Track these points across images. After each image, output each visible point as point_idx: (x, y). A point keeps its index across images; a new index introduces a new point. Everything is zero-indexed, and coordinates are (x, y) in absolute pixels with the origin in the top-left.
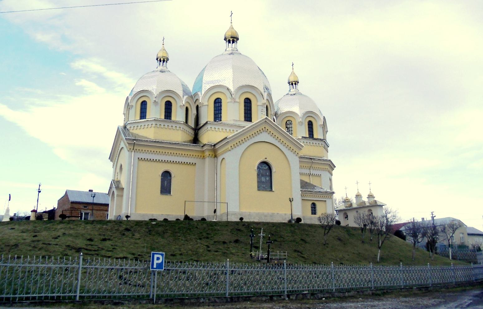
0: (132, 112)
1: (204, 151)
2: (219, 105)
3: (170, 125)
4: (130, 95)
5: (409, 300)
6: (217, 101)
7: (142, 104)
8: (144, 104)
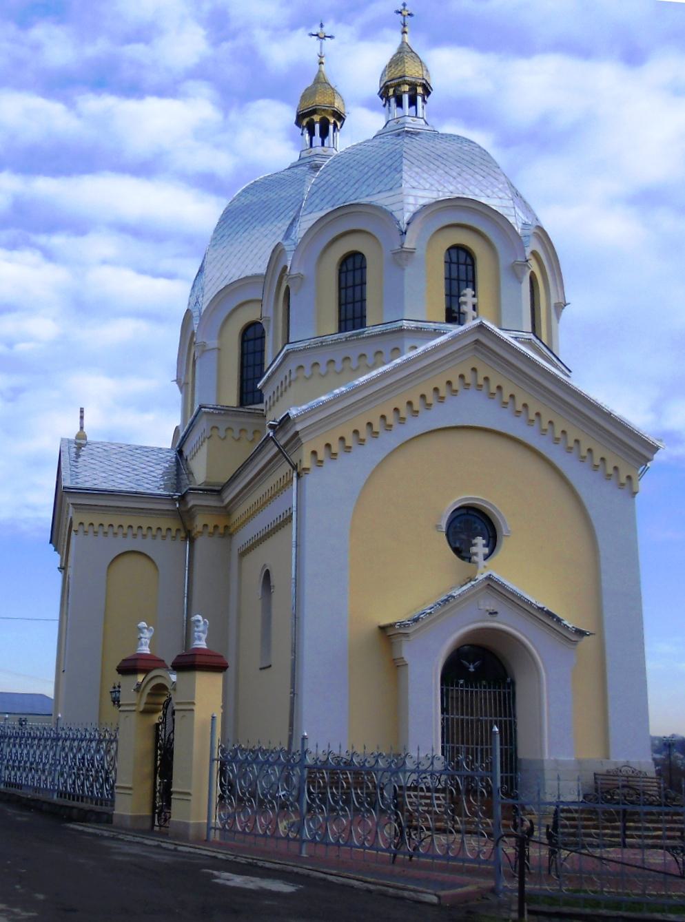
0: (206, 368)
1: (226, 507)
2: (358, 265)
4: (287, 236)
6: (250, 334)
7: (344, 268)
8: (350, 267)
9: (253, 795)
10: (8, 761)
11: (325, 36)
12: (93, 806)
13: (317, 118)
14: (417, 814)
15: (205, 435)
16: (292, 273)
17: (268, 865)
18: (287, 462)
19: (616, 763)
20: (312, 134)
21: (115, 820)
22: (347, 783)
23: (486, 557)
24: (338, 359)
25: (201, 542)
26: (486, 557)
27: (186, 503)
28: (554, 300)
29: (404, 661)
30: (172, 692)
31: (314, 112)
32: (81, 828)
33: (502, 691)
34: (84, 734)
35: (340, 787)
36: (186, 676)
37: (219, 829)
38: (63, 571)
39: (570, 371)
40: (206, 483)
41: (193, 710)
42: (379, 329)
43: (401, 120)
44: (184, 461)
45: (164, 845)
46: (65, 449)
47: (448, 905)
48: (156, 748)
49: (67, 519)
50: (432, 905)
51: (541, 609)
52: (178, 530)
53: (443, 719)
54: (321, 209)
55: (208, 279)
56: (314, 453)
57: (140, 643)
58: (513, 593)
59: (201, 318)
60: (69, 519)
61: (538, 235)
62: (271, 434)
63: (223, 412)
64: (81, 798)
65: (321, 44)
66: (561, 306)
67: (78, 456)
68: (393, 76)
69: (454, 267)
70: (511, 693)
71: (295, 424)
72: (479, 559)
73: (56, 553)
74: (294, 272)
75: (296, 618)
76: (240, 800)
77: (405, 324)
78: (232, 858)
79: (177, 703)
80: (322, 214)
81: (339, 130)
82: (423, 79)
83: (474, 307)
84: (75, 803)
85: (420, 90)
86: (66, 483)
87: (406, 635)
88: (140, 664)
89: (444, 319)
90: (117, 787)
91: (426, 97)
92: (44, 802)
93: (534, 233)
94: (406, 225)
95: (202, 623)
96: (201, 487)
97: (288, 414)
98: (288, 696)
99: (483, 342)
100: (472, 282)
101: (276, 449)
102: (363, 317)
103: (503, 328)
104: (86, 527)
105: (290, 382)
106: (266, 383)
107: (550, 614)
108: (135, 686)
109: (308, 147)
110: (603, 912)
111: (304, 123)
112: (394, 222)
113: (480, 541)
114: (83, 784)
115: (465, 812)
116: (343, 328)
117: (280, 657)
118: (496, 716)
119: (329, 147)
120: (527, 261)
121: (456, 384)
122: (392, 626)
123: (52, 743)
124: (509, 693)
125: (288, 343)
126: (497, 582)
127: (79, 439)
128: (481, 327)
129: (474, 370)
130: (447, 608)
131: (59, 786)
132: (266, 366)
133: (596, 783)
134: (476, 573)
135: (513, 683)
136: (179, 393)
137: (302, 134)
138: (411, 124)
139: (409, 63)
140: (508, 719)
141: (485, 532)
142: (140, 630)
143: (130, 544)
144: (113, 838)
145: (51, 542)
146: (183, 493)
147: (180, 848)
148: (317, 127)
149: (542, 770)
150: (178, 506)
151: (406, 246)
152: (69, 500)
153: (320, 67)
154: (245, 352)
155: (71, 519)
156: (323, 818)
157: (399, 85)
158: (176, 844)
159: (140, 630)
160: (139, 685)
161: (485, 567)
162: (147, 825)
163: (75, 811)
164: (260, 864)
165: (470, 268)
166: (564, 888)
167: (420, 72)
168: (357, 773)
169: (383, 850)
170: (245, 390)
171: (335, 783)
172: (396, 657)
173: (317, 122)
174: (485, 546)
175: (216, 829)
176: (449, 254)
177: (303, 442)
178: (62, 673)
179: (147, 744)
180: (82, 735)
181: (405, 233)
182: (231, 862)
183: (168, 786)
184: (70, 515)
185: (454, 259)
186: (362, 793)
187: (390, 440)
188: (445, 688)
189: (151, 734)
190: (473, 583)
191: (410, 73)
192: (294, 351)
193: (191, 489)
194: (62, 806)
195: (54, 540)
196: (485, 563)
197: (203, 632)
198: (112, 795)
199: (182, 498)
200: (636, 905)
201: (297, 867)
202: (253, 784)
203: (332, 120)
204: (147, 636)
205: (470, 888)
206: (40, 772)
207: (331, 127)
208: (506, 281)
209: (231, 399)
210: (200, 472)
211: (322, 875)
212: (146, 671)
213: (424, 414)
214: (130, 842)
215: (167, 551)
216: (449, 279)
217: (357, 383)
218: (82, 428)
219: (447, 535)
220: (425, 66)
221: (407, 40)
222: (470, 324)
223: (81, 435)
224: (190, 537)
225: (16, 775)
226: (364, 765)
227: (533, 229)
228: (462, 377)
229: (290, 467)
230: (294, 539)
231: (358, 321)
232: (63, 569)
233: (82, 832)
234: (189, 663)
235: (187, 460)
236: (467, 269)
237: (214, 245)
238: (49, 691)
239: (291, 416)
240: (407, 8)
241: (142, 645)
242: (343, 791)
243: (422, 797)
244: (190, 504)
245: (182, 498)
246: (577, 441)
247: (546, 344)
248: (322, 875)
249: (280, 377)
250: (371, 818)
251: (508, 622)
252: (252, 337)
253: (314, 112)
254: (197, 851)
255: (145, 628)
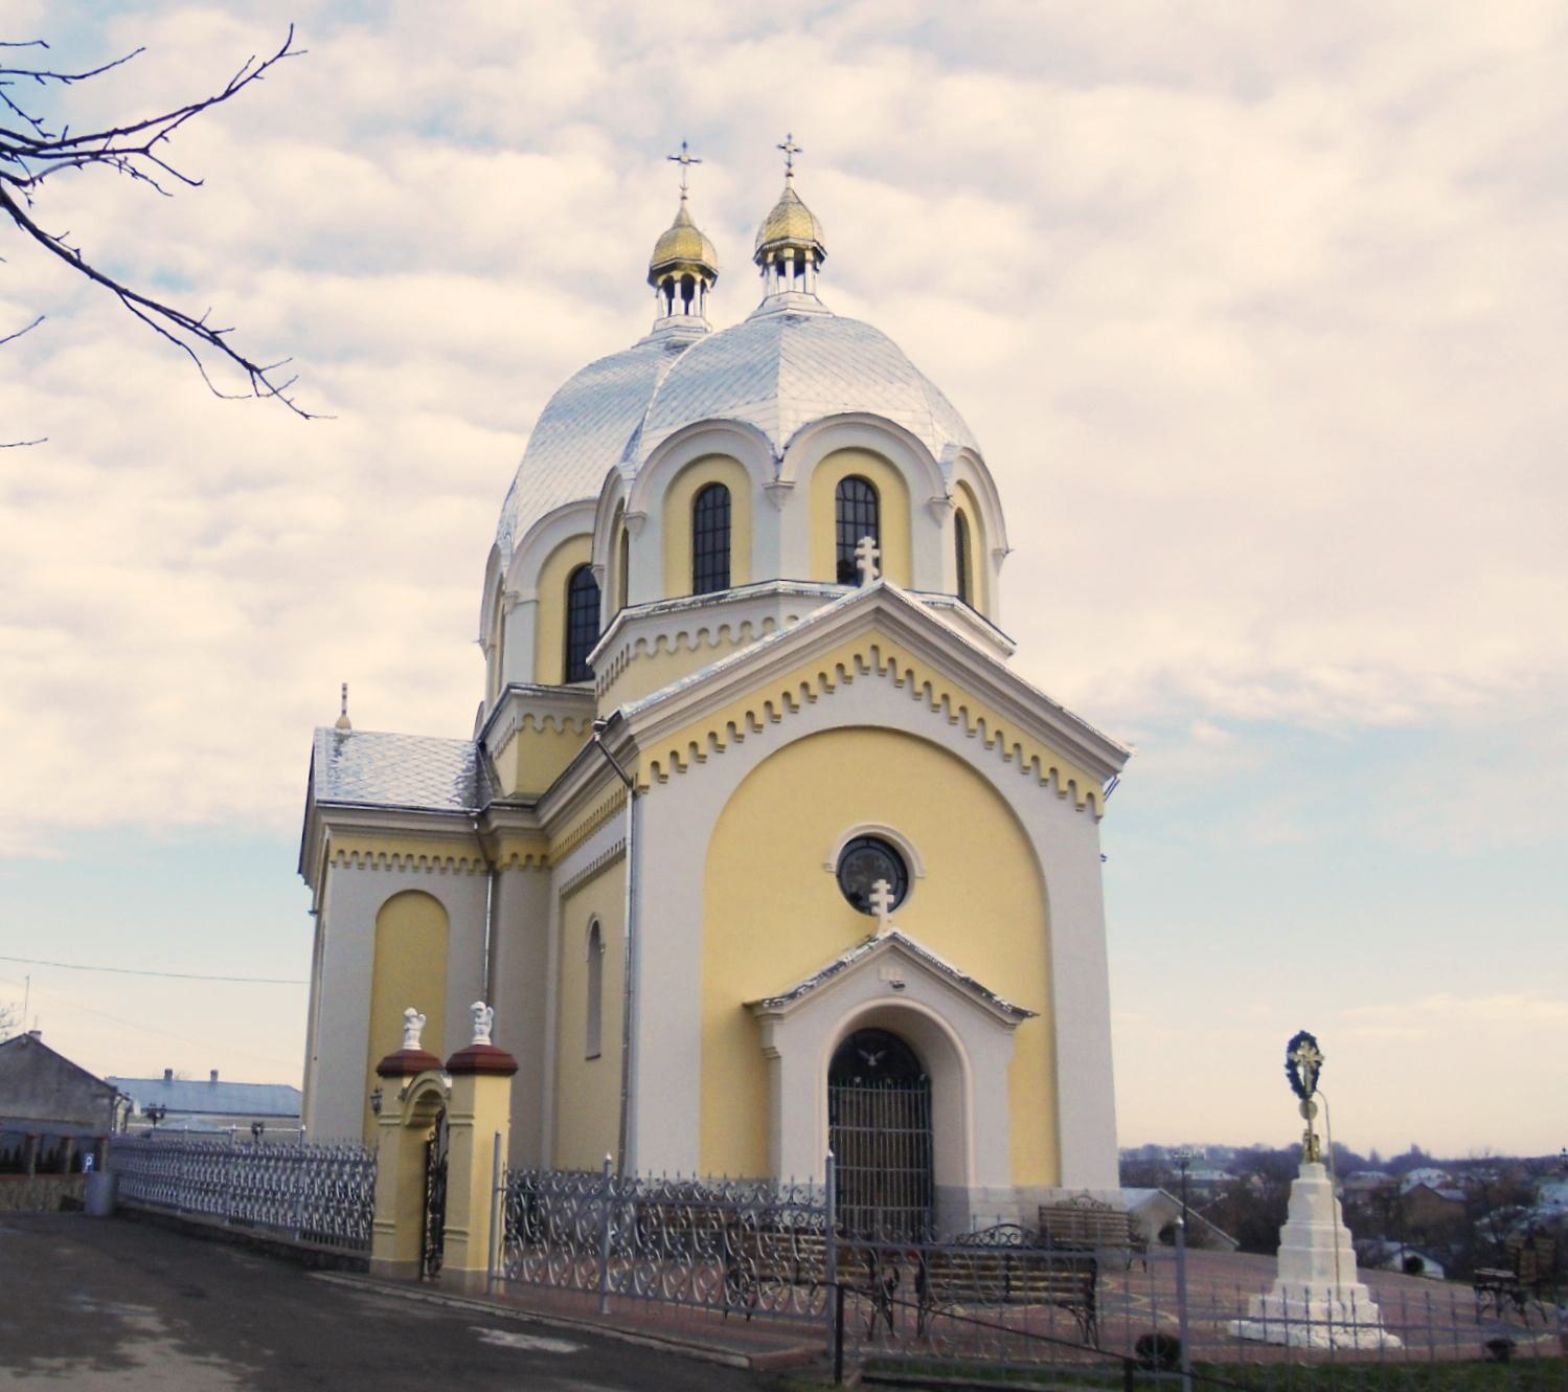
0: (519, 625)
2: (719, 500)
3: (734, 619)
4: (626, 457)
5: (223, 1221)
9: (571, 1236)
10: (235, 1188)
11: (690, 161)
12: (346, 1250)
13: (677, 275)
14: (807, 1265)
15: (515, 726)
16: (631, 511)
17: (555, 1323)
18: (618, 777)
19: (1070, 1192)
20: (670, 295)
21: (373, 1269)
22: (658, 1217)
23: (892, 908)
24: (692, 631)
25: (509, 880)
26: (892, 908)
27: (488, 823)
28: (991, 544)
29: (776, 1053)
30: (446, 1101)
31: (674, 266)
32: (327, 1278)
33: (913, 1092)
34: (334, 1153)
35: (678, 1225)
36: (465, 1081)
37: (502, 1278)
38: (316, 916)
39: (1014, 643)
40: (515, 795)
41: (470, 1125)
42: (749, 592)
43: (784, 297)
44: (487, 763)
45: (430, 1299)
46: (322, 744)
47: (762, 1369)
48: (427, 1173)
49: (322, 840)
50: (740, 1369)
51: (966, 981)
52: (477, 861)
53: (831, 1132)
54: (671, 424)
55: (524, 502)
56: (655, 765)
57: (407, 1036)
58: (927, 959)
59: (513, 557)
60: (325, 842)
61: (965, 458)
62: (598, 738)
63: (540, 694)
64: (333, 1239)
65: (684, 171)
66: (1001, 554)
67: (338, 753)
68: (773, 237)
69: (849, 506)
70: (926, 1095)
71: (628, 725)
72: (881, 910)
73: (307, 887)
74: (634, 510)
75: (630, 992)
76: (555, 1244)
77: (782, 587)
78: (513, 1314)
79: (454, 1116)
80: (673, 430)
81: (708, 292)
82: (814, 241)
83: (877, 562)
84: (323, 1246)
85: (809, 256)
86: (318, 796)
87: (779, 1017)
88: (406, 1064)
89: (834, 578)
90: (377, 1225)
91: (818, 264)
92: (282, 1245)
93: (962, 456)
94: (782, 451)
95: (485, 1012)
96: (509, 801)
97: (618, 712)
98: (618, 1098)
99: (888, 614)
100: (873, 528)
101: (603, 759)
102: (726, 573)
103: (917, 589)
104: (348, 857)
105: (628, 660)
106: (597, 658)
107: (977, 988)
108: (399, 1093)
109: (666, 315)
110: (955, 1380)
111: (660, 281)
112: (767, 446)
113: (882, 886)
114: (333, 1220)
115: (727, 1251)
116: (700, 591)
117: (612, 1043)
118: (904, 1127)
119: (695, 316)
120: (948, 498)
121: (850, 669)
122: (758, 1004)
123: (293, 1165)
124: (923, 1095)
125: (627, 607)
126: (905, 944)
127: (342, 728)
128: (883, 592)
129: (875, 648)
130: (835, 979)
131: (301, 1223)
132: (602, 629)
133: (1041, 1220)
134: (876, 929)
135: (928, 1082)
136: (484, 658)
137: (657, 297)
138: (798, 305)
139: (795, 219)
140: (920, 1131)
141: (892, 872)
142: (408, 1019)
143: (409, 881)
144: (367, 1291)
145: (300, 872)
146: (484, 807)
147: (451, 1303)
148: (678, 288)
149: (966, 1203)
150: (476, 826)
151: (782, 478)
152: (325, 819)
153: (683, 204)
154: (574, 606)
155: (328, 841)
156: (658, 1268)
157: (781, 248)
158: (445, 1298)
159: (408, 1019)
160: (405, 1091)
161: (890, 921)
162: (415, 1274)
163: (322, 1256)
164: (546, 1321)
165: (871, 507)
166: (956, 1355)
167: (810, 231)
168: (699, 1208)
169: (698, 1304)
170: (573, 660)
171: (672, 1221)
172: (766, 1047)
173: (677, 281)
174: (889, 892)
175: (499, 1279)
176: (843, 490)
177: (641, 749)
178: (313, 1061)
179: (415, 1167)
180: (332, 1154)
181: (781, 460)
182: (512, 1318)
183: (438, 1226)
184: (326, 837)
185: (850, 494)
186: (705, 1234)
187: (758, 747)
188: (834, 1089)
189: (421, 1154)
190: (872, 944)
191: (796, 232)
192: (633, 619)
193: (494, 804)
194: (306, 1250)
195: (305, 868)
196: (890, 916)
197: (486, 1024)
198: (371, 1235)
199: (483, 817)
200: (986, 1373)
201: (591, 1324)
202: (571, 1224)
203: (698, 277)
204: (416, 1027)
205: (796, 1351)
206: (277, 1204)
207: (697, 288)
208: (920, 522)
209: (553, 674)
210: (509, 776)
211: (619, 1335)
212: (414, 1073)
213: (806, 710)
214: (388, 1295)
215: (458, 890)
216: (842, 522)
217: (714, 668)
218: (344, 712)
219: (839, 876)
220: (818, 222)
221: (792, 186)
222: (869, 585)
223: (343, 723)
224: (493, 871)
225: (245, 1207)
226: (740, 1200)
227: (959, 452)
228: (858, 658)
229: (623, 783)
230: (628, 883)
231: (719, 579)
232: (317, 912)
233: (329, 1283)
234: (468, 1065)
235: (491, 757)
236: (867, 510)
237: (532, 455)
238: (298, 1083)
239: (623, 715)
240: (793, 141)
241: (409, 1038)
242: (682, 1230)
243: (816, 1243)
244: (495, 823)
245: (483, 817)
246: (1017, 746)
247: (982, 614)
248: (619, 1335)
249: (615, 653)
250: (716, 1266)
251: (921, 998)
252: (582, 588)
253: (674, 266)
254: (472, 1306)
255: (414, 1016)
